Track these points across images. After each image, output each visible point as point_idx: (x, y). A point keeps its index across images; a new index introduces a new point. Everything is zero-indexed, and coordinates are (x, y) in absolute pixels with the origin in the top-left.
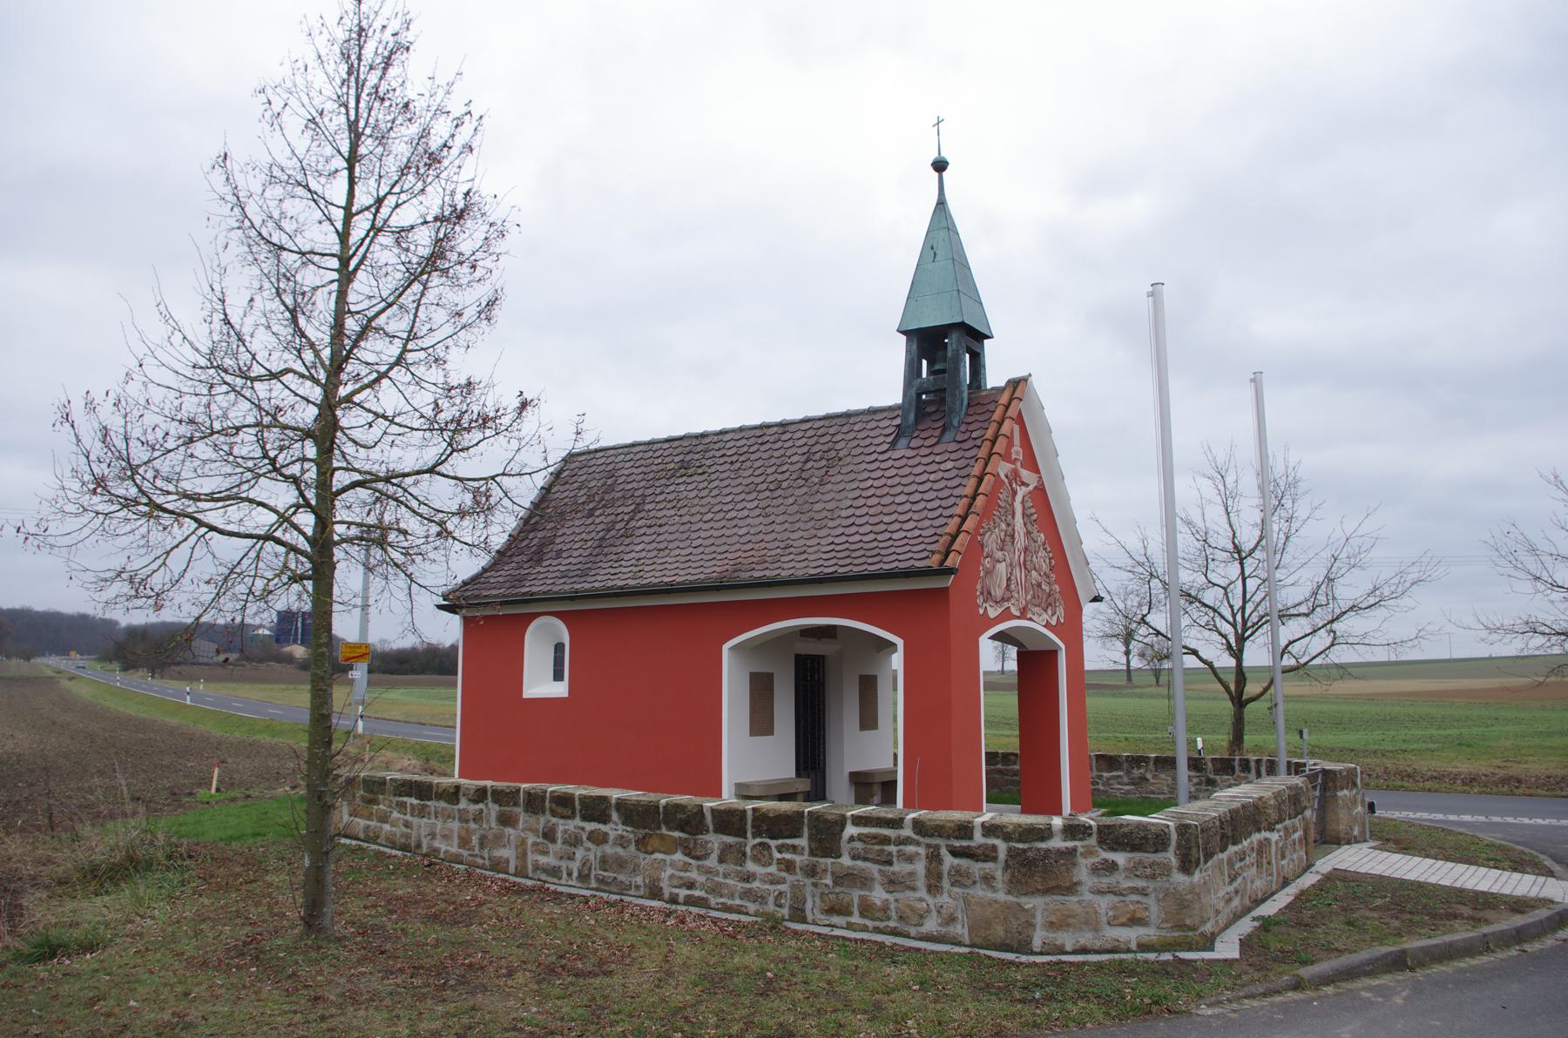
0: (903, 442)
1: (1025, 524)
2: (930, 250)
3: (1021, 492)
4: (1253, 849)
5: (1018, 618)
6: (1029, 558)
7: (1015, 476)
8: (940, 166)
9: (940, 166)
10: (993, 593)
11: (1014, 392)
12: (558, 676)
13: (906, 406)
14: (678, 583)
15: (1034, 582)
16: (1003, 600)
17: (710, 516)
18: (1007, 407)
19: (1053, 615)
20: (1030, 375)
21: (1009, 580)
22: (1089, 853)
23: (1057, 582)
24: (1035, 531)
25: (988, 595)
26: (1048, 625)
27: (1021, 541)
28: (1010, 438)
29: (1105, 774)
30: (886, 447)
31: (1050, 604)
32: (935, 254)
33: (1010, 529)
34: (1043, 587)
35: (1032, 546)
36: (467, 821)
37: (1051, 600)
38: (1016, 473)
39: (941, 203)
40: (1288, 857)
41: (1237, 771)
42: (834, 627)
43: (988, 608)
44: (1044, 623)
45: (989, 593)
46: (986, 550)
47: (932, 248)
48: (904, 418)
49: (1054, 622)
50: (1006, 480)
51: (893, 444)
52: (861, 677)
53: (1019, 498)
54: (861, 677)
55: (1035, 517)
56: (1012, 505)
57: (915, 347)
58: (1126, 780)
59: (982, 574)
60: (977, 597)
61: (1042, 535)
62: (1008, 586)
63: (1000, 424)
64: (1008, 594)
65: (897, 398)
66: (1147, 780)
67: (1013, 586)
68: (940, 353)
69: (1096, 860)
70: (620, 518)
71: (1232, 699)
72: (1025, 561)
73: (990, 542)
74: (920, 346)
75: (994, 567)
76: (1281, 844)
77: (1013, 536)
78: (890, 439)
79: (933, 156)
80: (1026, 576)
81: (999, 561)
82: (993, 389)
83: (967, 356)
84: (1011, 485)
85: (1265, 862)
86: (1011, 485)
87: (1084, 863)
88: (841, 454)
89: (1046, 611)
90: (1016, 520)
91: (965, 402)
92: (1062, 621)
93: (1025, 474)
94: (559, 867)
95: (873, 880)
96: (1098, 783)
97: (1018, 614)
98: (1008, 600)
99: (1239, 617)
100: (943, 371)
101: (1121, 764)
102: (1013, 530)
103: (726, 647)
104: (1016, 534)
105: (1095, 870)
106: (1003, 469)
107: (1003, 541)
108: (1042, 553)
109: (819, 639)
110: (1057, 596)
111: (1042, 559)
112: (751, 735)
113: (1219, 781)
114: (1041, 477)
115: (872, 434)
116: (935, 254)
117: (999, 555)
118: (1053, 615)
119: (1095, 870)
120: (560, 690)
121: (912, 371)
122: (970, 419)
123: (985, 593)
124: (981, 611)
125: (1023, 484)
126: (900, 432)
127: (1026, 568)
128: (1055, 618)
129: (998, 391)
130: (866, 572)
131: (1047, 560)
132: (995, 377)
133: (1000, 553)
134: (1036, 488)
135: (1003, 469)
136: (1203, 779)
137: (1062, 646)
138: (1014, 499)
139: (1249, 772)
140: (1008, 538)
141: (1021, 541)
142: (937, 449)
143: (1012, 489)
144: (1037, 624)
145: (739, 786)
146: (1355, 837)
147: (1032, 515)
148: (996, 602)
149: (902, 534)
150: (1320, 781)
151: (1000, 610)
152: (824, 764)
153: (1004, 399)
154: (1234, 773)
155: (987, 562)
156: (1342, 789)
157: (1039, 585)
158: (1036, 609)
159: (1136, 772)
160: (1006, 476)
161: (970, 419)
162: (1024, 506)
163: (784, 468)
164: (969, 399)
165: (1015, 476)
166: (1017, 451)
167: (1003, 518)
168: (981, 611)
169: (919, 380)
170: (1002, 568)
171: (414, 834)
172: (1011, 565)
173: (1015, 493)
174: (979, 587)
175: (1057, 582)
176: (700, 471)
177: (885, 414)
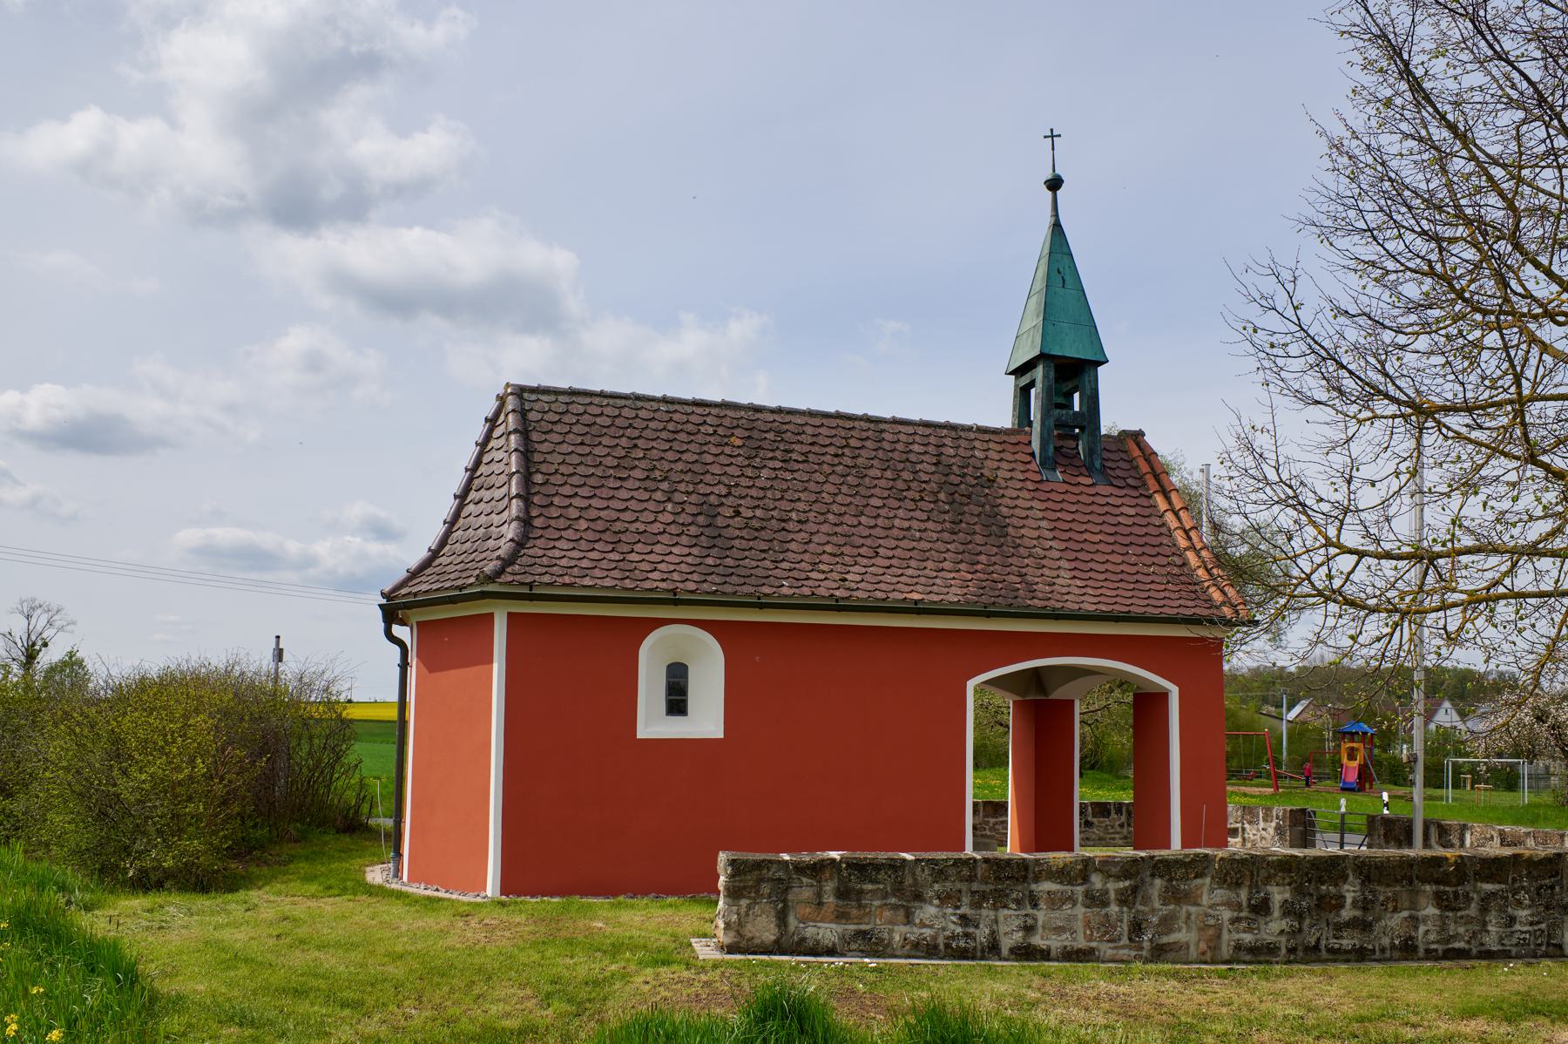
8: (1054, 184)
9: (1054, 184)
29: (992, 820)
39: (1057, 227)
47: (1059, 272)
79: (1048, 175)
96: (985, 829)
103: (971, 684)
154: (1109, 814)
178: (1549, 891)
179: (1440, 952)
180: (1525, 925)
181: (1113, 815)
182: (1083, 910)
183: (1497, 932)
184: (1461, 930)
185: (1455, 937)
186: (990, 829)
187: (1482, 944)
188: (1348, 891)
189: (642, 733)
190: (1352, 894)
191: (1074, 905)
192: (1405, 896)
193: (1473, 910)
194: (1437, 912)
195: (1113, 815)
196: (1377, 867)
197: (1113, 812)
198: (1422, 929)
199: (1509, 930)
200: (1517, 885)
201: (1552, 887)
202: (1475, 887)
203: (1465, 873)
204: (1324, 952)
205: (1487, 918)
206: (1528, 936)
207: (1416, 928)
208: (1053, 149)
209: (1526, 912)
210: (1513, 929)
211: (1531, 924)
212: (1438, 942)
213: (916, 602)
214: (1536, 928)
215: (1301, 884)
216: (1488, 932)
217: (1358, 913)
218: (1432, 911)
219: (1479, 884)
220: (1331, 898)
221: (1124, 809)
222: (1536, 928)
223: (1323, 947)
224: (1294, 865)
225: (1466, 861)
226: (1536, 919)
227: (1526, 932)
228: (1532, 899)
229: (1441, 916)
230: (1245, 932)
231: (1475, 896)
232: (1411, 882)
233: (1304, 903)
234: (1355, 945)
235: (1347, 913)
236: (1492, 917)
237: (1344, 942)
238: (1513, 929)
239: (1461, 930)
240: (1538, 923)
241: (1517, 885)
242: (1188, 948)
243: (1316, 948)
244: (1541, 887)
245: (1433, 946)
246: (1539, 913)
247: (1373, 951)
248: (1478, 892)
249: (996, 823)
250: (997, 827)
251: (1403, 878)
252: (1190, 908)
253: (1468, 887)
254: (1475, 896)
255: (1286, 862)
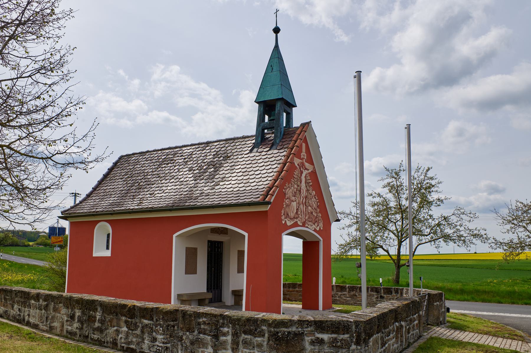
0: (255, 150)
1: (306, 187)
2: (270, 67)
3: (305, 173)
4: (394, 330)
5: (301, 226)
6: (307, 201)
7: (302, 165)
8: (277, 30)
9: (277, 30)
10: (289, 215)
11: (303, 128)
12: (108, 248)
13: (258, 134)
14: (155, 208)
15: (309, 211)
16: (294, 218)
17: (173, 180)
18: (299, 135)
19: (318, 226)
20: (310, 122)
21: (297, 209)
22: (311, 333)
23: (320, 212)
24: (311, 190)
25: (287, 216)
26: (315, 230)
27: (304, 193)
28: (300, 147)
29: (340, 293)
30: (248, 152)
31: (316, 221)
32: (272, 69)
33: (299, 188)
34: (314, 214)
35: (309, 196)
36: (41, 310)
37: (317, 220)
38: (303, 164)
39: (277, 46)
40: (411, 333)
41: (393, 293)
42: (227, 229)
43: (287, 221)
44: (313, 229)
45: (288, 214)
46: (287, 196)
47: (271, 66)
48: (256, 139)
49: (318, 229)
50: (298, 167)
51: (251, 151)
52: (239, 251)
53: (304, 175)
54: (239, 251)
55: (311, 184)
56: (300, 178)
57: (262, 109)
58: (348, 296)
59: (284, 206)
60: (281, 216)
61: (314, 192)
62: (297, 212)
63: (296, 141)
64: (297, 216)
65: (254, 133)
66: (356, 296)
67: (299, 213)
68: (273, 112)
69: (313, 338)
70: (137, 181)
71: (396, 264)
72: (305, 202)
73: (289, 192)
74: (264, 109)
75: (290, 203)
76: (408, 327)
77: (300, 191)
78: (250, 149)
79: (274, 26)
80: (306, 209)
81: (293, 201)
82: (295, 127)
83: (285, 114)
84: (300, 169)
85: (399, 335)
86: (300, 169)
87: (308, 339)
88: (229, 155)
89: (314, 224)
90: (302, 184)
91: (282, 133)
92: (322, 229)
93: (307, 165)
94: (76, 332)
95: (207, 344)
96: (336, 297)
97: (301, 224)
98: (297, 218)
99: (400, 234)
100: (273, 120)
101: (346, 289)
102: (301, 188)
103: (174, 236)
104: (302, 190)
105: (312, 343)
106: (297, 161)
107: (295, 193)
108: (314, 199)
109: (220, 234)
110: (320, 218)
111: (314, 202)
112: (186, 273)
113: (386, 297)
114: (314, 167)
115: (243, 146)
116: (272, 69)
117: (293, 198)
118: (317, 226)
119: (312, 343)
120: (108, 253)
121: (261, 119)
122: (284, 141)
123: (286, 214)
124: (283, 222)
125: (306, 169)
126: (255, 146)
127: (306, 205)
128: (318, 227)
129: (297, 128)
130: (233, 203)
131: (316, 203)
132: (296, 123)
133: (294, 198)
134: (312, 171)
135: (297, 161)
136: (379, 296)
137: (322, 239)
138: (301, 175)
139: (398, 294)
140: (298, 192)
141: (304, 193)
142: (269, 153)
143: (301, 171)
144: (310, 229)
145: (179, 296)
146: (441, 322)
147: (310, 183)
148: (291, 219)
149: (250, 188)
150: (427, 298)
151: (292, 222)
152: (221, 287)
153: (298, 132)
154: (392, 293)
155: (287, 201)
156: (436, 302)
157: (312, 213)
158: (310, 223)
159: (352, 293)
160: (298, 165)
161: (284, 140)
162: (306, 179)
163: (205, 161)
164: (284, 132)
165: (302, 165)
166: (304, 154)
167: (296, 183)
168: (283, 222)
169: (263, 123)
170: (294, 204)
171: (22, 314)
172: (299, 203)
173: (302, 173)
174: (283, 212)
175: (320, 212)
176: (172, 162)
177: (249, 139)
178: (172, 328)
179: (125, 348)
180: (161, 343)
181: (394, 294)
182: (38, 311)
183: (148, 344)
184: (134, 340)
185: (131, 343)
186: (339, 297)
187: (142, 348)
188: (98, 315)
189: (95, 255)
190: (99, 317)
191: (37, 309)
192: (115, 320)
193: (138, 332)
194: (127, 330)
195: (394, 294)
196: (105, 307)
197: (393, 292)
198: (120, 336)
199: (153, 344)
200: (158, 323)
201: (174, 326)
202: (140, 321)
203: (134, 314)
204: (89, 339)
205: (144, 336)
206: (161, 349)
207: (118, 336)
208: (276, 17)
209: (162, 337)
210: (154, 344)
211: (163, 343)
212: (124, 343)
213: (132, 209)
214: (165, 345)
215: (84, 310)
216: (144, 343)
217: (100, 325)
218: (125, 329)
219: (142, 320)
220: (93, 317)
221: (399, 291)
222: (165, 345)
223: (89, 337)
224: (81, 302)
225: (136, 308)
226: (165, 341)
227: (160, 347)
228: (163, 331)
229: (127, 332)
230: (69, 326)
231: (140, 325)
232: (117, 315)
233: (84, 318)
234: (99, 338)
235: (97, 325)
236: (146, 336)
237: (95, 336)
238: (154, 344)
239: (134, 340)
240: (166, 343)
241: (158, 323)
242: (57, 329)
243: (87, 337)
244: (169, 326)
245: (123, 345)
246: (167, 338)
247: (104, 342)
248: (142, 324)
249: (341, 295)
250: (341, 296)
251: (114, 312)
252: (58, 314)
253: (137, 321)
254: (140, 325)
255: (79, 300)
